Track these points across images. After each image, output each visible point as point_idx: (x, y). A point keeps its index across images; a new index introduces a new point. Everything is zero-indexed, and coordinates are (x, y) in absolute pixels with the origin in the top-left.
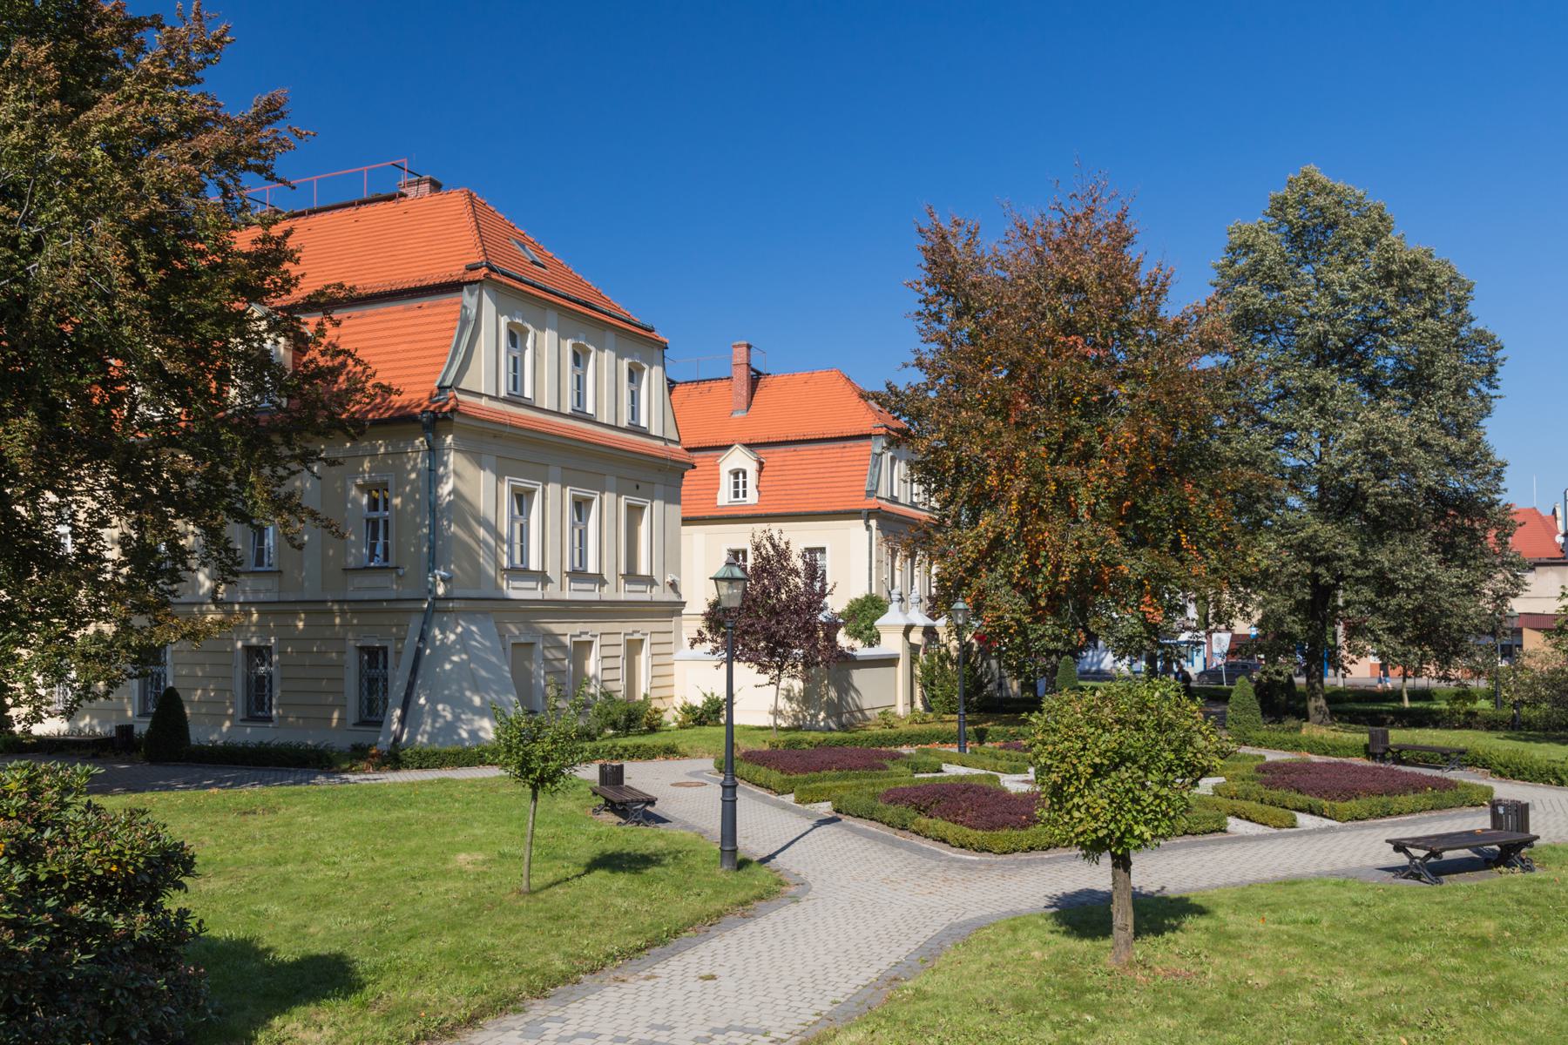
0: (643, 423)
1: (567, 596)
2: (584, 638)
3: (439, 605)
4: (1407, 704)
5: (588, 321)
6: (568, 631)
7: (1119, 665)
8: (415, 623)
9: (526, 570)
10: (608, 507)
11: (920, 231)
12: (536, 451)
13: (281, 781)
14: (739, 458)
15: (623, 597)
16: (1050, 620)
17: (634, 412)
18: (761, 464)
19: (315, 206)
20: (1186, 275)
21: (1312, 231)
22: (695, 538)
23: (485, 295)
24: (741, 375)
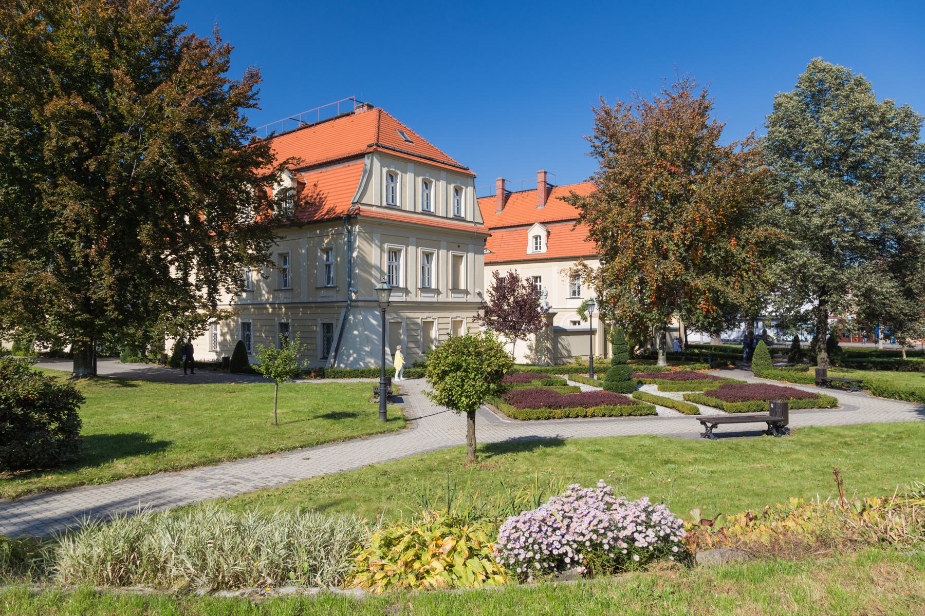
0: (463, 215)
1: (419, 299)
2: (429, 320)
3: (353, 304)
4: (905, 357)
5: (430, 167)
6: (420, 317)
7: (791, 338)
8: (343, 311)
9: (398, 287)
10: (442, 258)
11: (594, 110)
12: (397, 230)
13: (251, 382)
14: (538, 230)
15: (450, 300)
16: (655, 311)
17: (459, 210)
18: (549, 233)
19: (319, 121)
20: (743, 126)
21: (816, 96)
22: (489, 271)
23: (375, 159)
24: (541, 188)
